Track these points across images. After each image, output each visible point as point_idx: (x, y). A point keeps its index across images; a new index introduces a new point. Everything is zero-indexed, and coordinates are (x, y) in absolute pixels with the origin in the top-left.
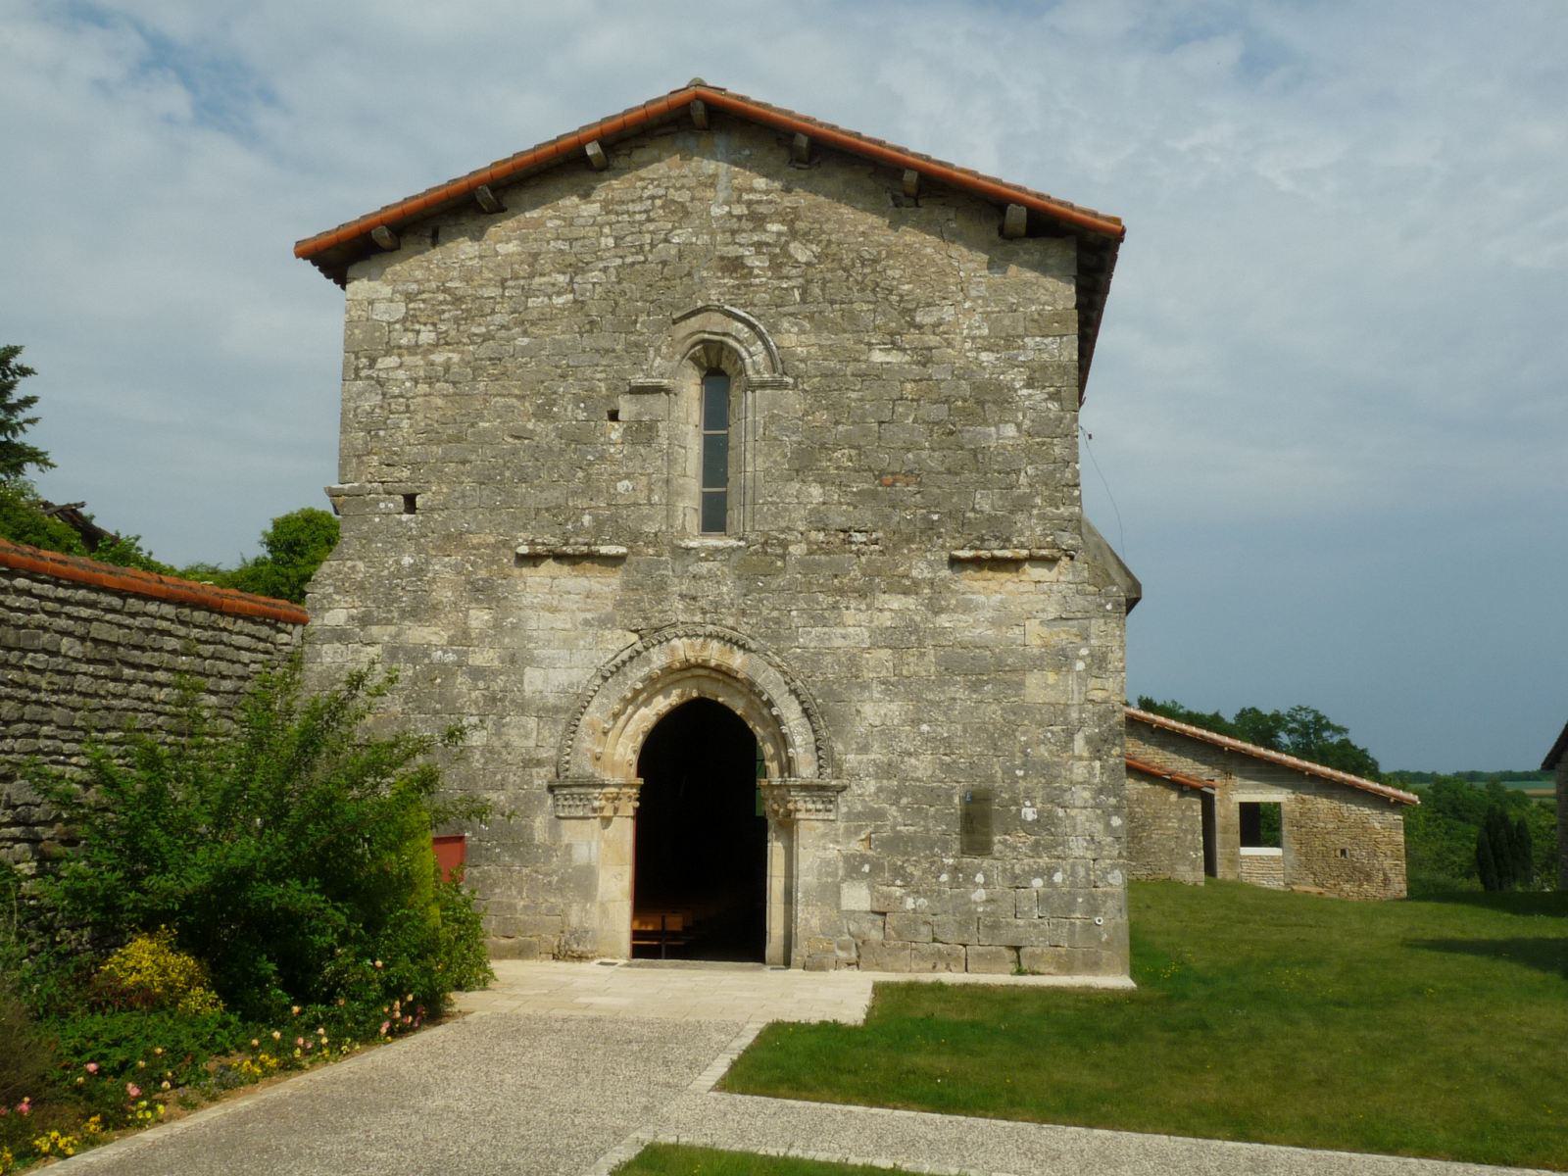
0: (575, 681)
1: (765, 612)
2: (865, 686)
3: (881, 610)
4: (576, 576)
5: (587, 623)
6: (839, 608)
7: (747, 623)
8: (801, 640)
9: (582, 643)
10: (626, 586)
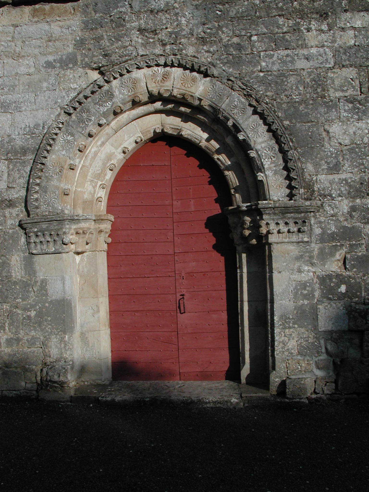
0: (41, 123)
1: (225, 40)
2: (331, 105)
3: (343, 29)
4: (36, 22)
5: (49, 65)
6: (299, 29)
7: (208, 52)
8: (264, 64)
9: (45, 85)
10: (86, 26)
